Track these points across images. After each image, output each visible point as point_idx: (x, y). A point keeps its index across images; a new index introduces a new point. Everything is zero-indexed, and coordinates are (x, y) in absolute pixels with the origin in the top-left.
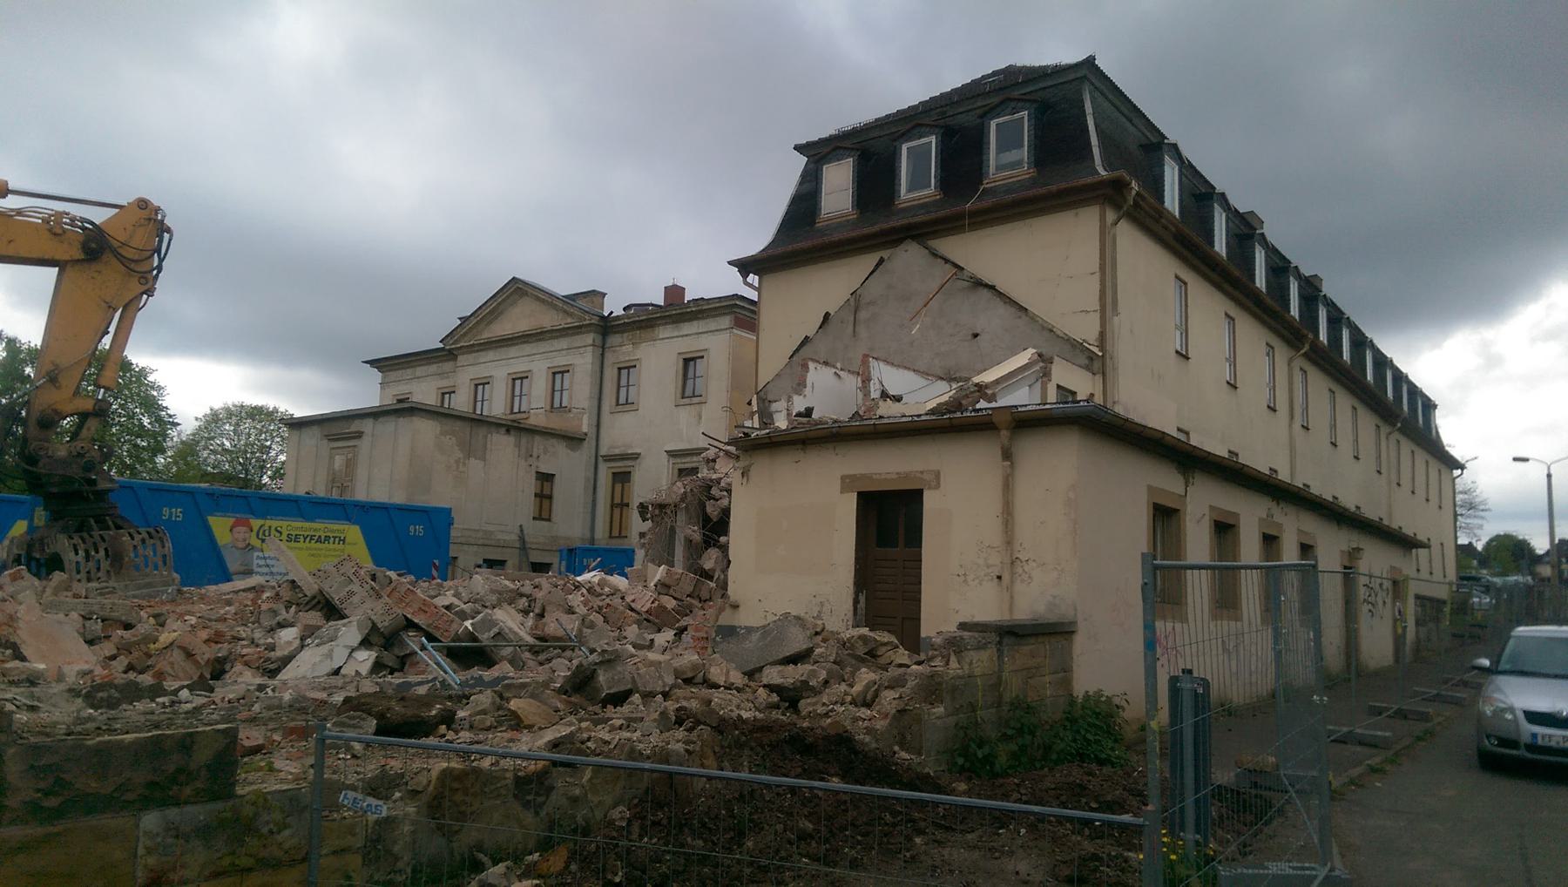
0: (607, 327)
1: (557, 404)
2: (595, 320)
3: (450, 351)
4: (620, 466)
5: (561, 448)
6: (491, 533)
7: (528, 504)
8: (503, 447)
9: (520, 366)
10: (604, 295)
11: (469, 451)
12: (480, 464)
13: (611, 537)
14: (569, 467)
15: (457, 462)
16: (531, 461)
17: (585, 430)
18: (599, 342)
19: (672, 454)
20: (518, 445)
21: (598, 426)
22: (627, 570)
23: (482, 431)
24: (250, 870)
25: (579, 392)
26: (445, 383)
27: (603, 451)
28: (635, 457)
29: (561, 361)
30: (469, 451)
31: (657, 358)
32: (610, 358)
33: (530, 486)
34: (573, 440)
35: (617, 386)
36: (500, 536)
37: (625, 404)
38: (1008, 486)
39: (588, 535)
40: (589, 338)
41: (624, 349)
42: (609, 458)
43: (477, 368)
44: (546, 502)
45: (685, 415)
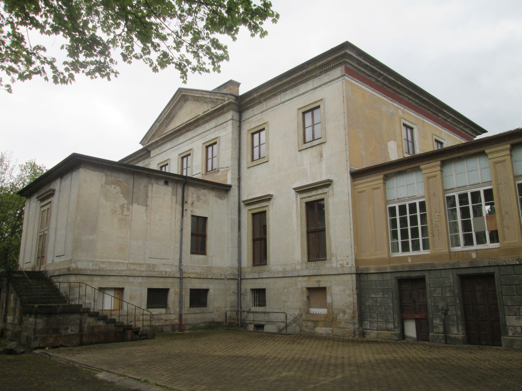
1: (210, 169)
2: (232, 100)
4: (257, 208)
5: (211, 197)
6: (154, 265)
8: (163, 196)
9: (184, 148)
11: (131, 198)
12: (142, 209)
14: (220, 215)
15: (122, 207)
17: (229, 183)
18: (236, 117)
19: (300, 191)
21: (239, 179)
23: (143, 182)
25: (224, 156)
27: (244, 198)
28: (268, 198)
29: (210, 137)
30: (131, 198)
31: (280, 119)
34: (223, 189)
35: (250, 151)
36: (162, 268)
37: (258, 160)
39: (236, 265)
40: (230, 115)
41: (254, 118)
42: (249, 203)
43: (161, 156)
45: (308, 156)
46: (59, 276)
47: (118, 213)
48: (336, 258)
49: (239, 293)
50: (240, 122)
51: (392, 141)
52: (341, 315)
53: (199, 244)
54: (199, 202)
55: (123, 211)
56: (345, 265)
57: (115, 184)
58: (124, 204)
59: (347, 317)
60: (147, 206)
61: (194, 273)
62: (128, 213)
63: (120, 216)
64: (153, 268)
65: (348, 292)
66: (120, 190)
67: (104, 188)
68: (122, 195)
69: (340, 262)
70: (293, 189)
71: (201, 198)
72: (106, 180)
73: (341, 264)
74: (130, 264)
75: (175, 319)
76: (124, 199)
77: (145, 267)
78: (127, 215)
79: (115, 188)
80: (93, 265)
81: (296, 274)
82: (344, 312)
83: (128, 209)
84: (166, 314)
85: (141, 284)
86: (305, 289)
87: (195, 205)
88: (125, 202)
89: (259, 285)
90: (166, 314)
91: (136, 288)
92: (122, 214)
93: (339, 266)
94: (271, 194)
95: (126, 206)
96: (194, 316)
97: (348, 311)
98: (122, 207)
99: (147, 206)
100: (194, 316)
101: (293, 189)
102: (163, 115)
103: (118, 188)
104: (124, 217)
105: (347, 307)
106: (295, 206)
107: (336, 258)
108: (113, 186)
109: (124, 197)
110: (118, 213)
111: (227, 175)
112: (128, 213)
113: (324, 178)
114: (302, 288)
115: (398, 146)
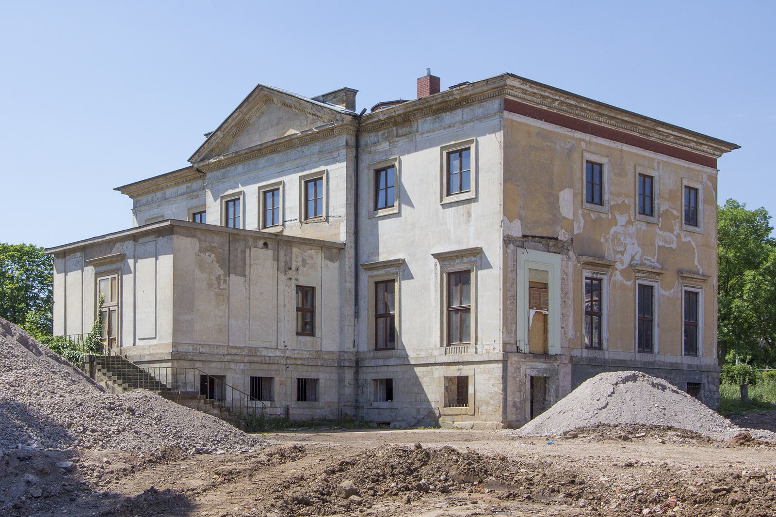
0: (360, 125)
3: (198, 170)
7: (290, 319)
10: (355, 92)
12: (240, 279)
13: (377, 349)
15: (218, 278)
16: (291, 274)
18: (352, 141)
20: (277, 259)
21: (356, 233)
22: (633, 360)
24: (725, 494)
26: (195, 202)
32: (366, 160)
33: (290, 300)
35: (377, 189)
36: (265, 353)
38: (156, 261)
44: (381, 311)
46: (149, 362)
47: (215, 286)
48: (482, 343)
49: (358, 385)
50: (357, 146)
51: (567, 189)
52: (484, 407)
53: (307, 325)
54: (305, 267)
55: (219, 283)
56: (491, 351)
57: (209, 251)
58: (220, 275)
59: (490, 408)
60: (245, 276)
61: (301, 359)
62: (225, 286)
63: (217, 290)
64: (255, 353)
65: (493, 381)
66: (215, 258)
67: (198, 257)
68: (217, 265)
69: (486, 347)
70: (436, 256)
71: (307, 261)
72: (200, 247)
73: (486, 350)
74: (231, 347)
75: (281, 414)
76: (220, 268)
77: (247, 351)
78: (224, 289)
79: (210, 256)
80: (193, 349)
81: (432, 361)
82: (488, 404)
83: (225, 281)
84: (271, 407)
85: (243, 371)
86: (443, 379)
87: (300, 271)
88: (221, 272)
89: (384, 374)
90: (271, 407)
91: (238, 376)
92: (219, 289)
93: (484, 352)
94: (400, 256)
95: (222, 277)
96: (301, 411)
97: (492, 402)
98: (218, 278)
99: (245, 276)
100: (299, 411)
101: (436, 256)
102: (230, 121)
103: (213, 256)
104: (221, 291)
105: (491, 398)
106: (433, 276)
107: (482, 343)
108: (207, 254)
109: (220, 266)
110: (215, 286)
111: (339, 227)
112: (225, 286)
113: (472, 245)
114: (440, 377)
115: (575, 195)
